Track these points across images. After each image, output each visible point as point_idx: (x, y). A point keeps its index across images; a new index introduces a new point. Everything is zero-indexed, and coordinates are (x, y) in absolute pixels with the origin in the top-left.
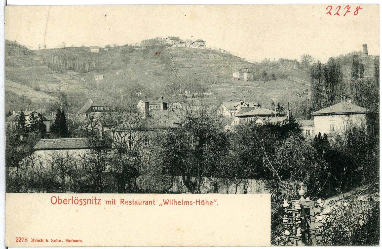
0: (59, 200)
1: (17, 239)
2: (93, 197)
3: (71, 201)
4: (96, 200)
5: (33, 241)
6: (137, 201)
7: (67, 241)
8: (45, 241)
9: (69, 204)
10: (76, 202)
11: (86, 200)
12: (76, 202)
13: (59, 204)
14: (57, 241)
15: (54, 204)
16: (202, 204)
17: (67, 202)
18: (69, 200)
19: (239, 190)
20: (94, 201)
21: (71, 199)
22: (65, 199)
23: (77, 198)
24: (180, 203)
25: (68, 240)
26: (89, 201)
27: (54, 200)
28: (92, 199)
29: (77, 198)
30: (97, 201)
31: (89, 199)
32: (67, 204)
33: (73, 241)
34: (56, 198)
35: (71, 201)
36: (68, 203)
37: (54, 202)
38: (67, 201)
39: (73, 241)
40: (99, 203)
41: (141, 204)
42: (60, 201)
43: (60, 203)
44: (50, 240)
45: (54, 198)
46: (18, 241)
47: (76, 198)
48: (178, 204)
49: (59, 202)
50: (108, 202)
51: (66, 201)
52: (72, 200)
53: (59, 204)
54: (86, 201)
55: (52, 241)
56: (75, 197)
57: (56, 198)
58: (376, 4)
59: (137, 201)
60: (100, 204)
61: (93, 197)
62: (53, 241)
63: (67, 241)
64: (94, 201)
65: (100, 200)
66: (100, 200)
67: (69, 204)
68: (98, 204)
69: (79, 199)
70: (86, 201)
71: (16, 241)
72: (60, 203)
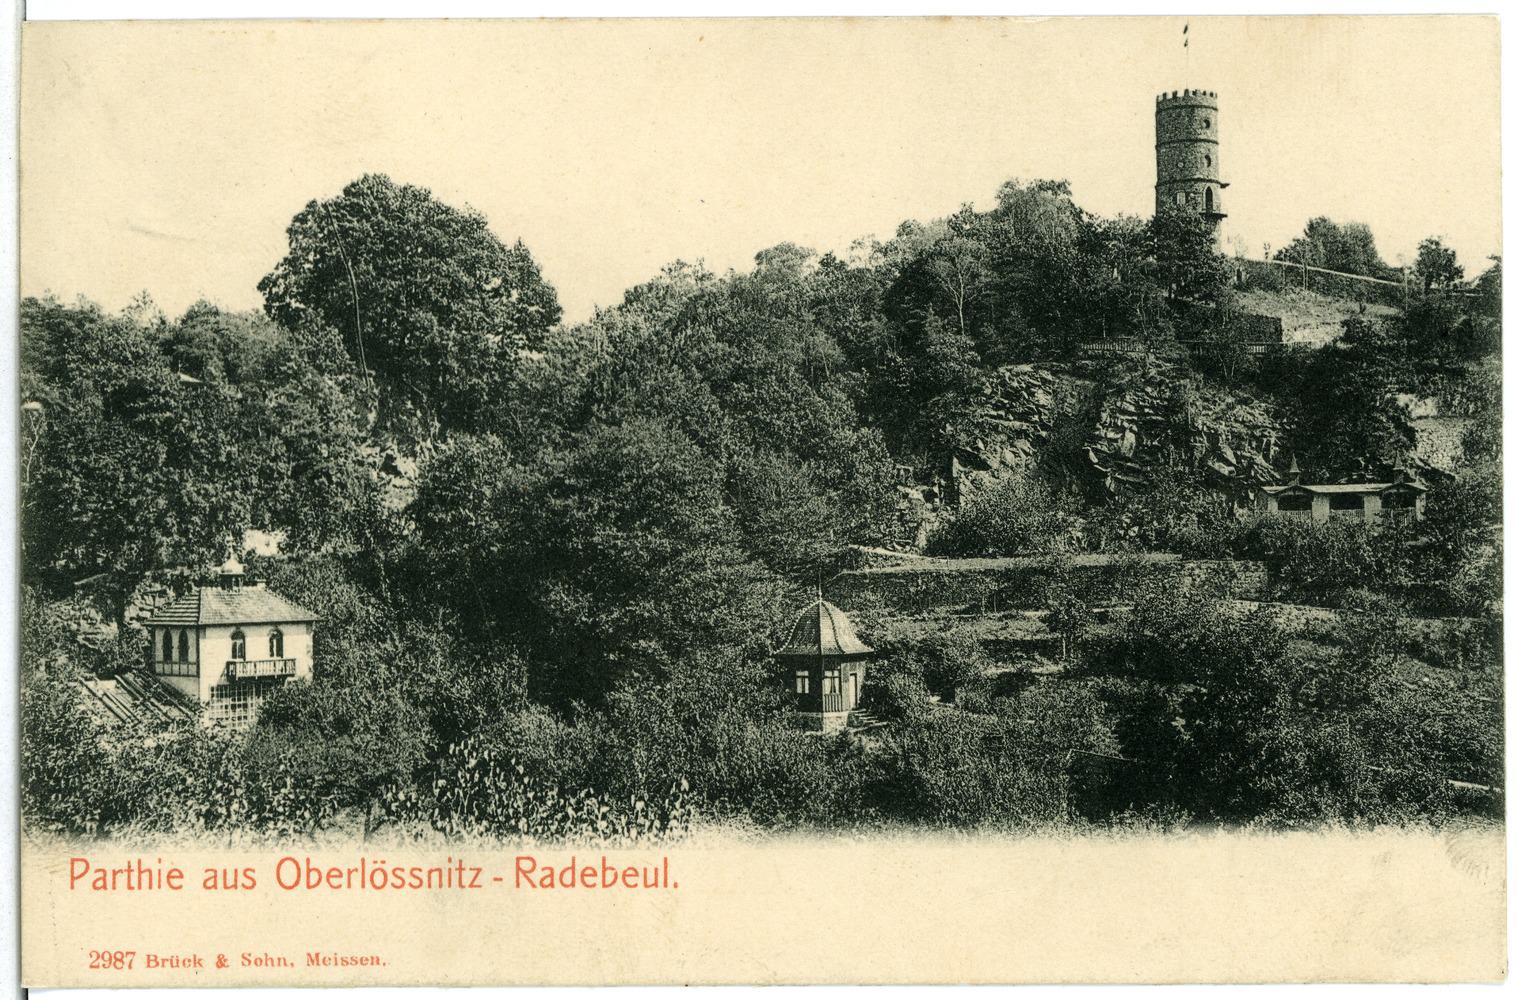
0: (309, 871)
1: (95, 956)
2: (450, 860)
3: (356, 878)
4: (461, 869)
5: (153, 964)
6: (216, 871)
7: (314, 959)
8: (210, 962)
9: (349, 886)
10: (379, 879)
11: (403, 870)
12: (379, 879)
13: (309, 887)
14: (265, 961)
15: (291, 888)
16: (375, 886)
17: (344, 881)
18: (350, 872)
19: (600, 334)
20: (455, 876)
21: (356, 870)
22: (334, 869)
23: (383, 862)
24: (595, 874)
25: (317, 955)
26: (435, 875)
27: (289, 873)
28: (448, 866)
29: (383, 862)
30: (468, 876)
31: (351, 868)
32: (594, 885)
33: (339, 962)
34: (299, 869)
35: (356, 878)
36: (345, 886)
37: (289, 879)
38: (341, 875)
39: (339, 962)
40: (476, 883)
41: (656, 884)
42: (314, 877)
43: (312, 882)
44: (233, 959)
45: (288, 863)
46: (98, 967)
47: (378, 866)
48: (328, 881)
49: (310, 877)
50: (212, 881)
51: (335, 876)
52: (360, 870)
53: (309, 887)
54: (424, 876)
55: (246, 962)
56: (375, 862)
57: (299, 869)
58: (830, 984)
59: (551, 869)
60: (479, 886)
61: (450, 860)
62: (250, 962)
63: (314, 959)
64: (455, 876)
65: (479, 870)
66: (479, 870)
67: (349, 886)
68: (471, 886)
69: (389, 870)
70: (424, 876)
71: (92, 967)
72: (312, 882)
